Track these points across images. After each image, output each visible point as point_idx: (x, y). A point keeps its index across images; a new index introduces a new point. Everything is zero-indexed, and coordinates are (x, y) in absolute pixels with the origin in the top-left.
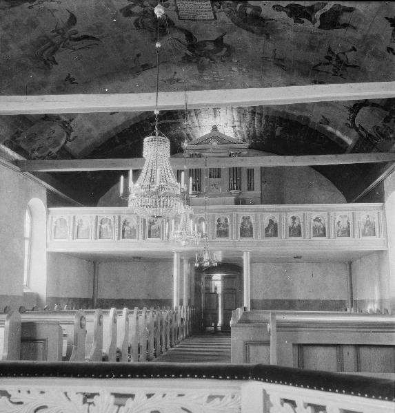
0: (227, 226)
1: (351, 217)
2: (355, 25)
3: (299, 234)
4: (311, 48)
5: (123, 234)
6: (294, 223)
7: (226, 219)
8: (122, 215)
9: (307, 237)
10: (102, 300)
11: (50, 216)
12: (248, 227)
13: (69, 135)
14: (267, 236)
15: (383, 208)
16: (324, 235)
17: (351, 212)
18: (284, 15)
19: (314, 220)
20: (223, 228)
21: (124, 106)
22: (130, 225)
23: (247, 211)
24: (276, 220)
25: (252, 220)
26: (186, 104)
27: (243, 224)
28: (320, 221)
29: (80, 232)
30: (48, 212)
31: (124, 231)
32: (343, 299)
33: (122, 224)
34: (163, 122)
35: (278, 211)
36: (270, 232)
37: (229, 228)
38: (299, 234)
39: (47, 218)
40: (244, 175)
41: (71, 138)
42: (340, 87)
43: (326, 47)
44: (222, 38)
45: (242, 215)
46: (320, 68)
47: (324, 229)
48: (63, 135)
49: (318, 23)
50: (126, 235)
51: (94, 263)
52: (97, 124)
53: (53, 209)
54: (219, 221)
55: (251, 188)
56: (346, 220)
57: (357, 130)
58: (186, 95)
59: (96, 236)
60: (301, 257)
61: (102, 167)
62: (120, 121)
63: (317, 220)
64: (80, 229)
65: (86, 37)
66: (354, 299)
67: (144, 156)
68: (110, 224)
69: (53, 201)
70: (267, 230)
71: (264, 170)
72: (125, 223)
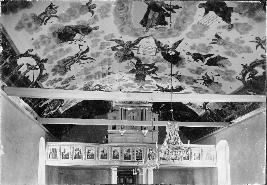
0: (141, 154)
1: (201, 151)
2: (224, 65)
4: (197, 72)
7: (141, 150)
8: (62, 147)
11: (47, 146)
15: (215, 147)
17: (201, 149)
18: (190, 57)
22: (91, 152)
30: (46, 144)
31: (88, 155)
33: (87, 152)
34: (172, 104)
39: (45, 147)
43: (205, 73)
44: (154, 64)
46: (198, 81)
47: (188, 157)
49: (206, 62)
50: (89, 157)
54: (137, 151)
56: (198, 152)
57: (206, 110)
59: (60, 158)
65: (89, 58)
68: (80, 151)
72: (89, 151)
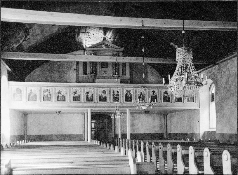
0: (118, 95)
5: (58, 99)
6: (153, 94)
7: (118, 92)
9: (173, 102)
10: (30, 136)
13: (26, 37)
16: (169, 101)
19: (164, 93)
21: (59, 21)
23: (128, 87)
24: (145, 93)
25: (131, 92)
26: (143, 26)
27: (127, 94)
29: (30, 97)
30: (8, 83)
32: (162, 133)
37: (119, 96)
40: (121, 68)
41: (26, 39)
42: (52, 15)
48: (23, 37)
50: (59, 99)
51: (25, 115)
52: (42, 32)
53: (11, 82)
54: (113, 92)
55: (125, 74)
58: (142, 20)
61: (29, 57)
62: (55, 30)
64: (30, 96)
66: (169, 132)
67: (176, 60)
69: (11, 78)
71: (132, 65)
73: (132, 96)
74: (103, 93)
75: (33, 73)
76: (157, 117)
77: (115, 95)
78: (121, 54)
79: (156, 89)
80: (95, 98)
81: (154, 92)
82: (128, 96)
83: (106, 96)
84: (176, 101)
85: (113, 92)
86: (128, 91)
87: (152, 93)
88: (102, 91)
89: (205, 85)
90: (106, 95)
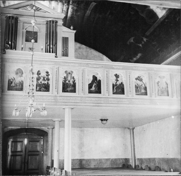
3: (123, 92)
6: (117, 80)
12: (71, 83)
14: (90, 92)
19: (136, 79)
20: (43, 82)
25: (145, 80)
28: (141, 80)
35: (124, 68)
36: (93, 88)
38: (123, 92)
45: (136, 74)
47: (145, 88)
54: (39, 73)
60: (107, 120)
63: (139, 79)
70: (90, 86)
73: (76, 82)
74: (17, 74)
75: (26, 126)
76: (118, 132)
77: (42, 78)
78: (73, 16)
79: (122, 71)
80: (52, 84)
81: (117, 76)
82: (67, 82)
83: (22, 81)
84: (158, 94)
85: (39, 73)
86: (68, 73)
87: (115, 78)
88: (15, 70)
89: (72, 76)
90: (22, 79)
